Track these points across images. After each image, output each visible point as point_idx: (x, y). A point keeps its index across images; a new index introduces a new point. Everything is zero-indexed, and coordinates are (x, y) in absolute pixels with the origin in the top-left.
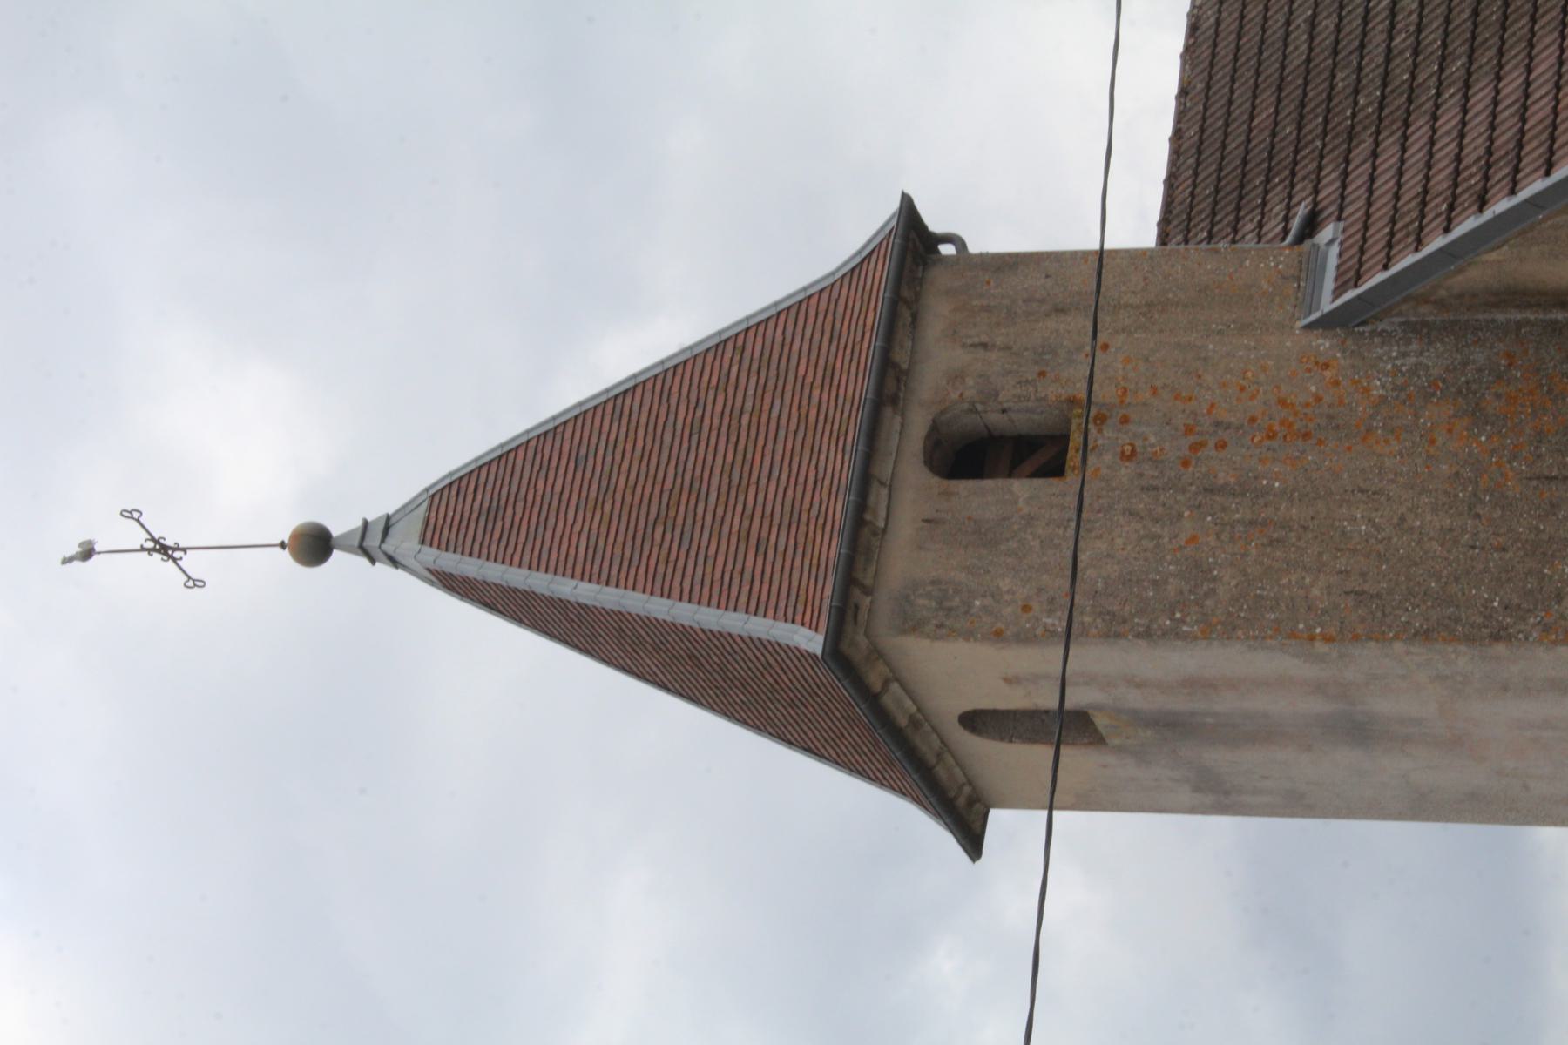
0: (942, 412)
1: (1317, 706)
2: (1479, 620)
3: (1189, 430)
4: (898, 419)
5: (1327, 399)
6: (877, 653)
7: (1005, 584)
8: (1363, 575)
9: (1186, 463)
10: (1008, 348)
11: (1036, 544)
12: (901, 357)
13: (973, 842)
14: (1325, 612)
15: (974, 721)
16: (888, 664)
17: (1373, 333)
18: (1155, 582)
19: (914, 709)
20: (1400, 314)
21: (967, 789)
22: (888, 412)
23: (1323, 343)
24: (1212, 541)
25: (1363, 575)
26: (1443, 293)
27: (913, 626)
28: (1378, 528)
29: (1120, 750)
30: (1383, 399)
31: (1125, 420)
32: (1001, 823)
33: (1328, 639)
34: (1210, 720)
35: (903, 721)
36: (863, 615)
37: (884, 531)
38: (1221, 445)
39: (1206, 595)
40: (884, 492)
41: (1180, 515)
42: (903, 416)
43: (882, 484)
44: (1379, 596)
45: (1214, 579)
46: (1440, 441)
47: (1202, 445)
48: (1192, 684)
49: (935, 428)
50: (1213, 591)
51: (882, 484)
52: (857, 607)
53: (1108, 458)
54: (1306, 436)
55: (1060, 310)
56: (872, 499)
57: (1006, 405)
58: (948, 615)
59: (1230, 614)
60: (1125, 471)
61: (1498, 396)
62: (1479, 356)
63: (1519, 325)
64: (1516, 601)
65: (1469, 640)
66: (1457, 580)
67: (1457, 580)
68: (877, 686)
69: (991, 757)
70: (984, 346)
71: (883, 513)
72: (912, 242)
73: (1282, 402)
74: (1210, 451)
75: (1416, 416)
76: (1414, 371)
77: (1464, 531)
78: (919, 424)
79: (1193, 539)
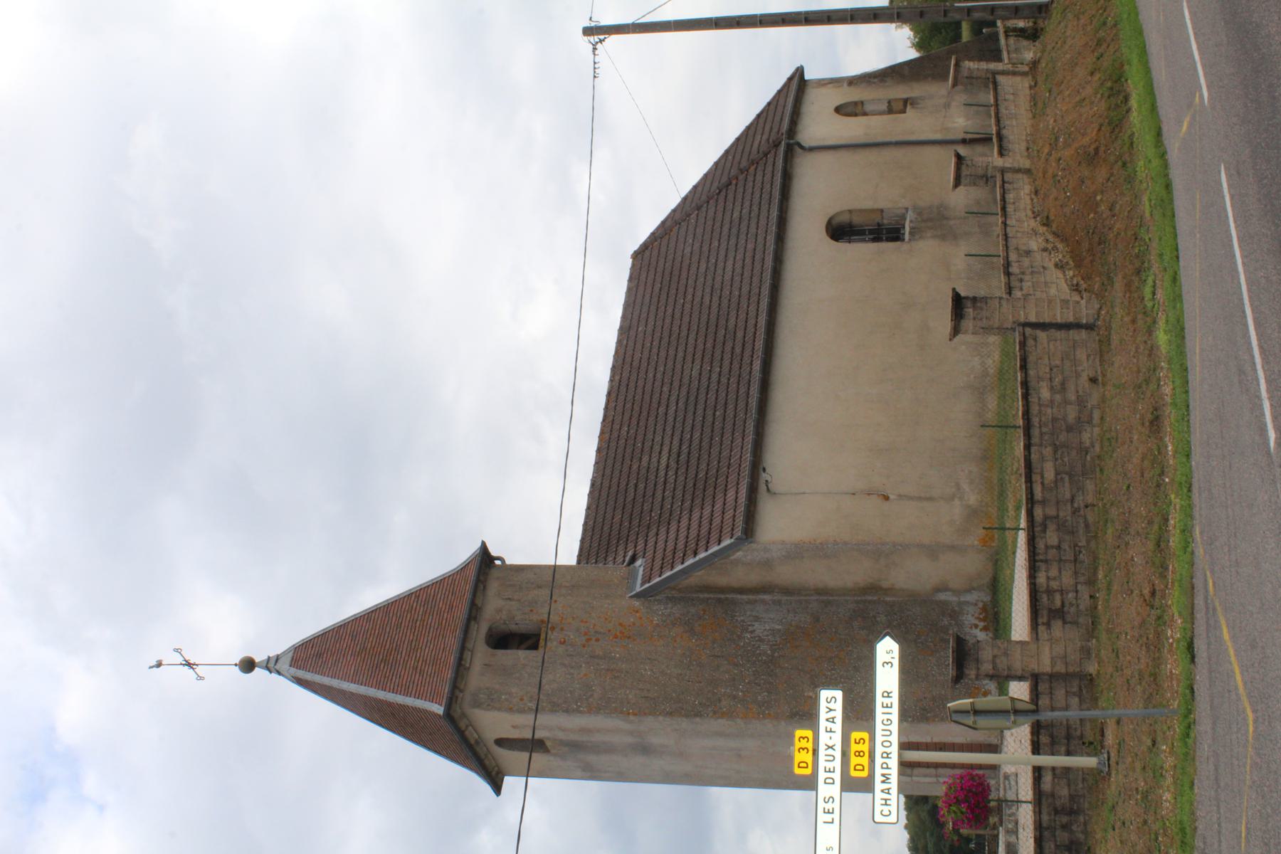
3: (586, 634)
6: (464, 715)
12: (478, 602)
15: (500, 742)
23: (637, 603)
27: (477, 704)
29: (555, 755)
31: (562, 629)
33: (635, 714)
35: (472, 742)
48: (583, 730)
58: (492, 701)
60: (561, 649)
62: (693, 610)
65: (687, 716)
72: (485, 559)
74: (593, 642)
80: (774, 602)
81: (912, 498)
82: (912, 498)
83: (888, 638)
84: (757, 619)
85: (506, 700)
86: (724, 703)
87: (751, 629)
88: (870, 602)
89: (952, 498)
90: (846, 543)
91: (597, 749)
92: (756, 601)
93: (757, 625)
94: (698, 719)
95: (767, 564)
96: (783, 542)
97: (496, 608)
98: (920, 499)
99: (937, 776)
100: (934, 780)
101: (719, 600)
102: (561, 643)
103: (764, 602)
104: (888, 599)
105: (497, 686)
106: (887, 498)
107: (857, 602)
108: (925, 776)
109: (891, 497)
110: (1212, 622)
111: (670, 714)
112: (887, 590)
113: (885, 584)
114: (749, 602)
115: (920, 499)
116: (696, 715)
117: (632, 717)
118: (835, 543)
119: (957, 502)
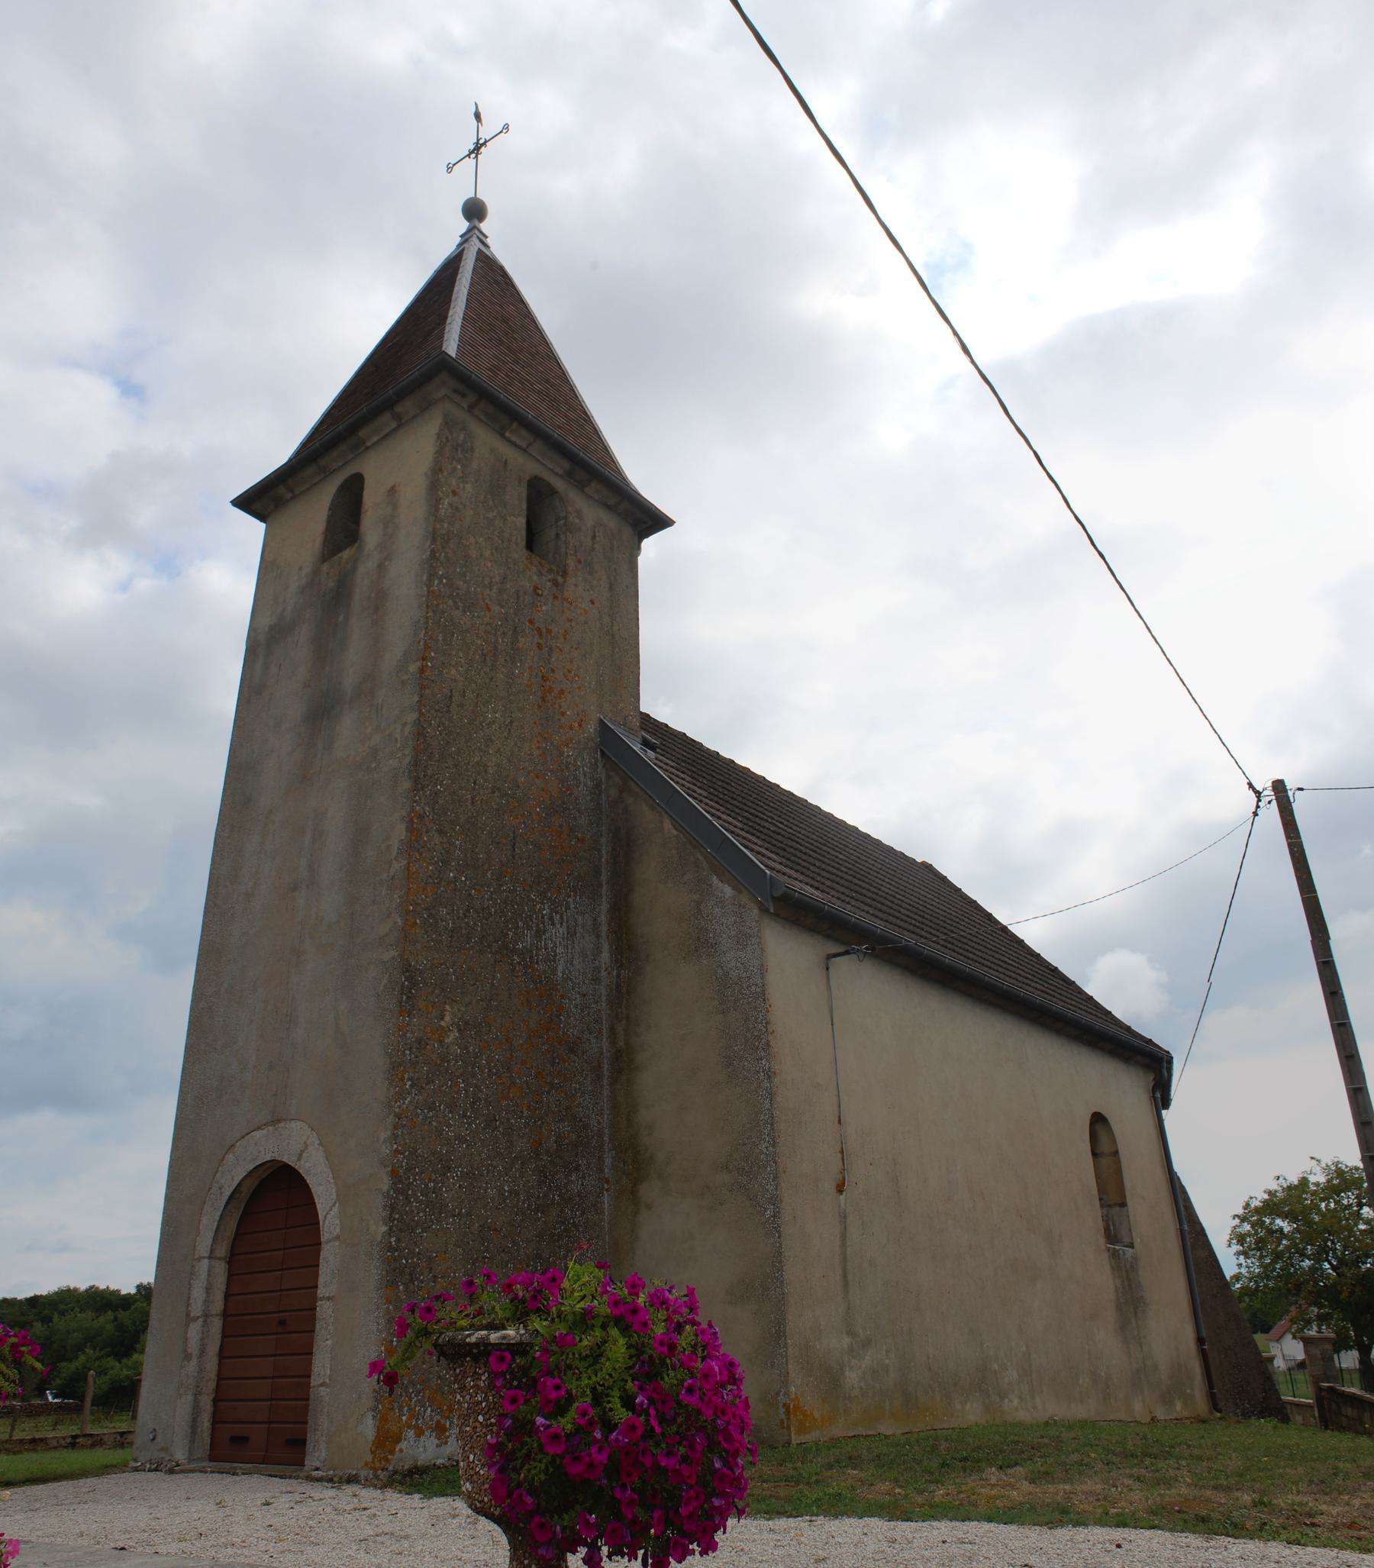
0: (561, 499)
1: (350, 679)
2: (429, 772)
3: (549, 632)
4: (561, 472)
5: (563, 720)
6: (425, 408)
7: (469, 487)
8: (461, 706)
9: (531, 622)
10: (593, 549)
11: (490, 515)
12: (594, 488)
13: (252, 502)
14: (441, 673)
15: (353, 489)
16: (415, 417)
17: (597, 760)
18: (464, 575)
19: (368, 444)
20: (608, 777)
21: (289, 495)
22: (567, 465)
23: (592, 728)
24: (487, 620)
25: (461, 706)
26: (630, 800)
27: (448, 424)
28: (490, 724)
29: (316, 572)
30: (562, 754)
31: (555, 597)
32: (253, 530)
33: (422, 670)
34: (341, 618)
35: (363, 433)
36: (457, 398)
37: (502, 435)
38: (540, 647)
39: (455, 603)
40: (524, 445)
41: (502, 607)
42: (561, 476)
43: (530, 444)
44: (448, 711)
45: (464, 612)
46: (538, 782)
47: (540, 635)
48: (379, 601)
49: (553, 492)
50: (457, 608)
51: (530, 444)
52: (464, 395)
53: (535, 578)
54: (543, 699)
55: (611, 587)
56: (524, 432)
57: (563, 537)
58: (452, 449)
59: (443, 612)
60: (527, 585)
61: (561, 826)
62: (583, 821)
63: (599, 851)
64: (441, 802)
65: (416, 763)
66: (455, 766)
67: (455, 766)
68: (398, 409)
69: (313, 514)
70: (594, 537)
71: (513, 439)
72: (653, 521)
73: (562, 692)
74: (537, 639)
75: (551, 771)
76: (576, 778)
77: (485, 780)
78: (559, 484)
79: (489, 609)
80: (597, 970)
81: (844, 1237)
82: (844, 1237)
83: (148, 1277)
84: (571, 933)
85: (455, 469)
86: (437, 839)
87: (557, 918)
88: (601, 1159)
89: (851, 1333)
90: (771, 1096)
91: (326, 648)
92: (598, 936)
93: (563, 930)
94: (407, 785)
95: (701, 944)
96: (763, 969)
97: (586, 512)
98: (844, 1259)
99: (206, 1315)
100: (197, 1309)
101: (597, 872)
102: (536, 588)
103: (598, 951)
104: (606, 1199)
105: (475, 465)
106: (840, 1189)
107: (600, 1135)
108: (208, 1290)
109: (842, 1197)
110: (55, 1443)
111: (420, 733)
112: (634, 1192)
113: (649, 1191)
114: (596, 924)
115: (844, 1259)
116: (416, 781)
117: (413, 668)
118: (770, 1075)
119: (846, 1341)
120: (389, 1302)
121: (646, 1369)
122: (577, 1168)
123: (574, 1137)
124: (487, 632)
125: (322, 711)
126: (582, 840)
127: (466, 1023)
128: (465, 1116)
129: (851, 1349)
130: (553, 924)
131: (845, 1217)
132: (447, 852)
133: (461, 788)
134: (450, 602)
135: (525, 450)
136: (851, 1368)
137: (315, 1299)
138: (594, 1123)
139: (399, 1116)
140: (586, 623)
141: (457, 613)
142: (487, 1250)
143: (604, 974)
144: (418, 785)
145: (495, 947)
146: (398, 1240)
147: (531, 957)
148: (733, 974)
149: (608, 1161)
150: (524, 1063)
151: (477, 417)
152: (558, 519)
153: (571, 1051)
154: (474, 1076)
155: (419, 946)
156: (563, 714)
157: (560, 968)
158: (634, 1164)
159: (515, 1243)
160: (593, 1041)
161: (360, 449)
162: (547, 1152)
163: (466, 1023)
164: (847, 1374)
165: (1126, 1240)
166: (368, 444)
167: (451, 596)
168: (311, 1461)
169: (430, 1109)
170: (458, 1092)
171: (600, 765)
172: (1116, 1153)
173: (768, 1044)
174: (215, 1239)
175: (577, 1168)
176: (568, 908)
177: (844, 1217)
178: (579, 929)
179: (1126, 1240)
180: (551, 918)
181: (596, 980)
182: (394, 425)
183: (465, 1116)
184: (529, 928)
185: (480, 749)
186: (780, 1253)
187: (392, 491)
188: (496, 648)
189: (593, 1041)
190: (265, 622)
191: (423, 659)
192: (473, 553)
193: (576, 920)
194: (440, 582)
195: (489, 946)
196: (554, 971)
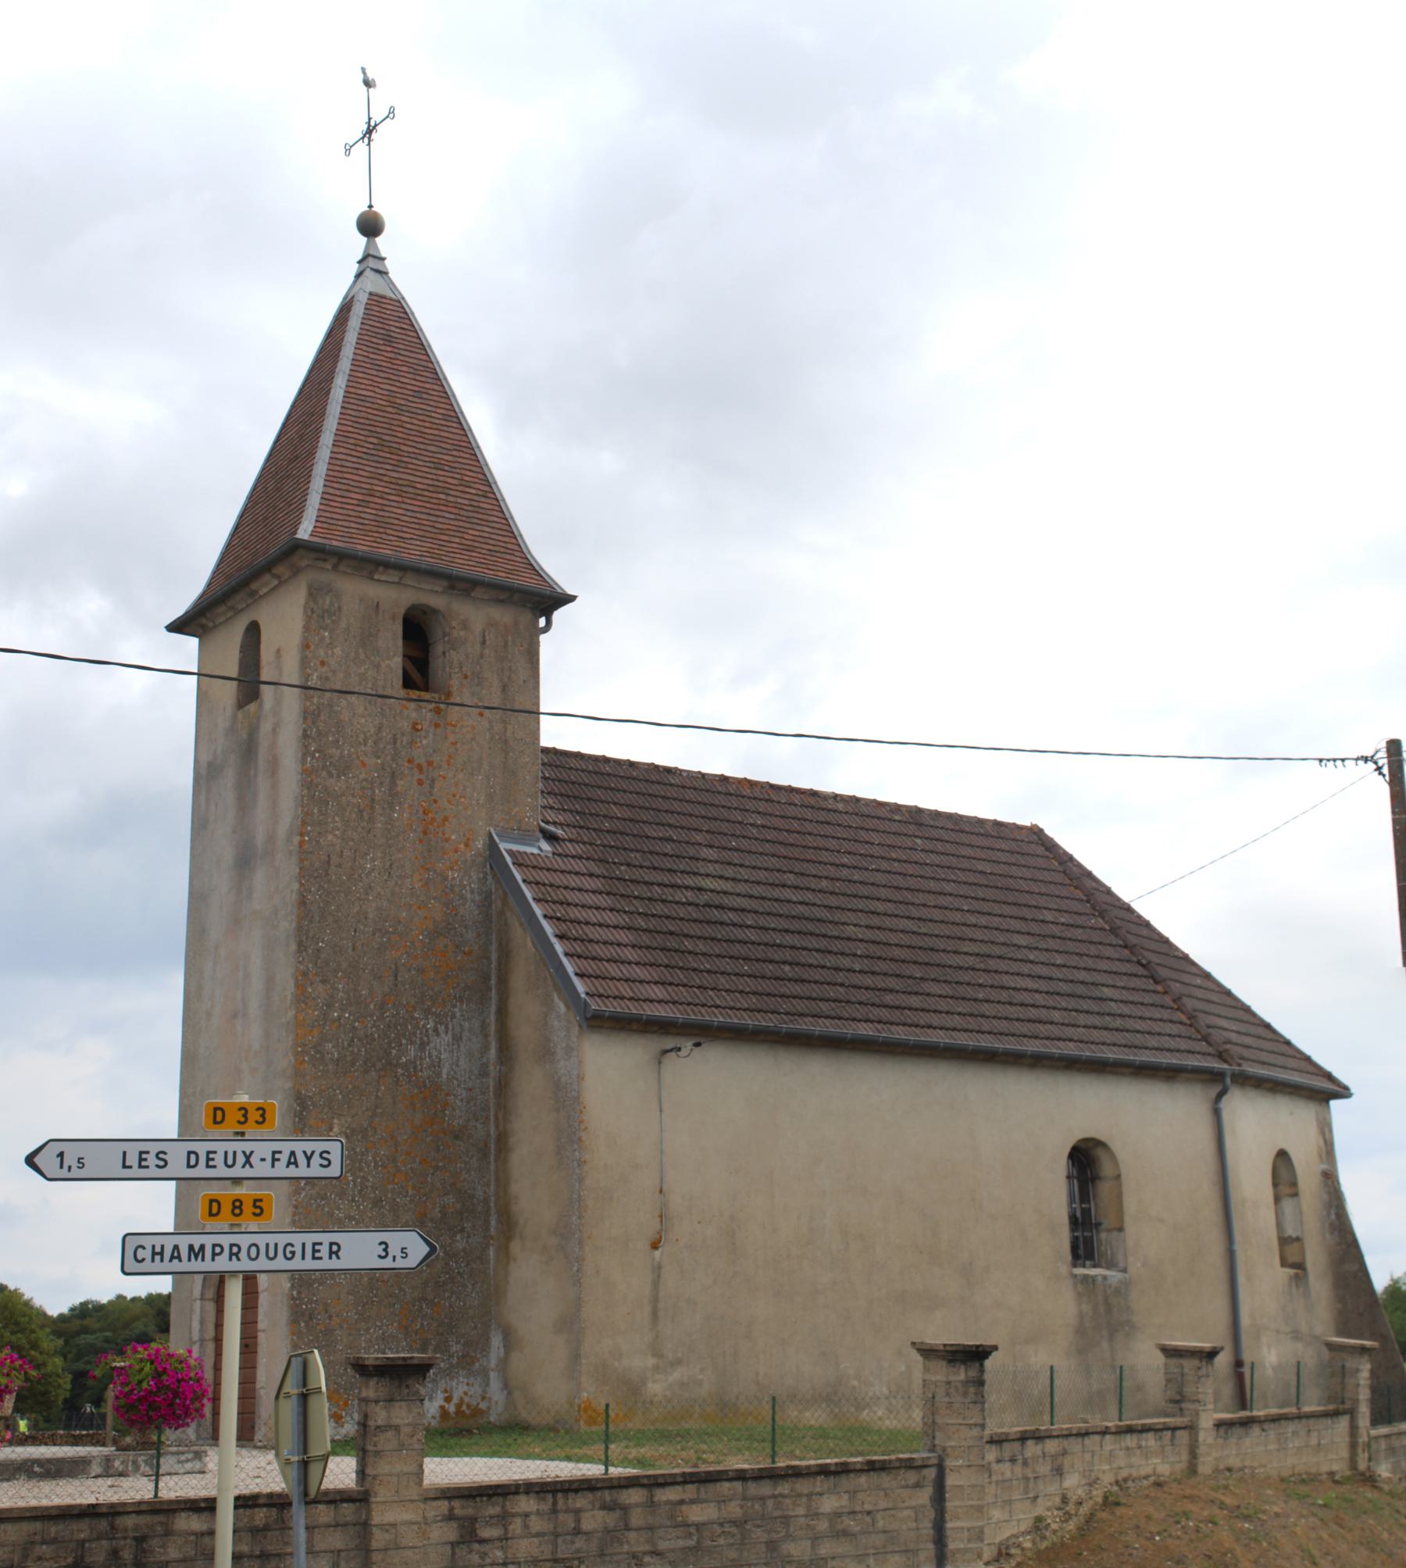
1: (260, 838)
3: (430, 763)
6: (296, 572)
7: (338, 651)
8: (339, 866)
10: (482, 656)
12: (478, 593)
19: (261, 593)
22: (445, 583)
27: (313, 593)
29: (235, 717)
30: (446, 879)
31: (437, 726)
32: (191, 644)
33: (301, 844)
36: (320, 564)
37: (372, 579)
38: (420, 782)
40: (396, 579)
44: (327, 874)
45: (339, 777)
48: (274, 765)
52: (325, 560)
53: (414, 715)
56: (391, 571)
58: (319, 616)
62: (470, 935)
63: (489, 959)
66: (336, 922)
69: (232, 638)
72: (549, 600)
73: (446, 819)
77: (365, 926)
79: (364, 765)
80: (485, 1065)
84: (457, 1039)
85: (322, 639)
87: (441, 1028)
88: (487, 1222)
92: (486, 1036)
93: (448, 1038)
95: (546, 1053)
96: (581, 1078)
97: (470, 622)
99: (202, 1341)
100: (196, 1336)
101: (486, 978)
103: (486, 1048)
104: (491, 1252)
107: (486, 1201)
108: (202, 1322)
109: (657, 1253)
111: (302, 902)
112: (507, 1248)
113: (515, 1247)
114: (484, 1026)
117: (296, 839)
118: (581, 1163)
119: (650, 1362)
120: (293, 1334)
121: (157, 1376)
122: (462, 1230)
123: (458, 1206)
124: (363, 788)
125: (244, 862)
126: (470, 953)
127: (353, 1131)
128: (353, 1200)
129: (656, 1369)
130: (438, 1035)
131: (660, 1267)
132: (332, 996)
133: (342, 939)
134: (324, 773)
135: (398, 583)
136: (655, 1381)
137: (256, 1331)
138: (479, 1193)
139: (296, 1207)
140: (473, 739)
141: (332, 781)
142: (376, 1296)
143: (491, 1068)
144: (301, 947)
145: (379, 1065)
146: (299, 1293)
147: (415, 1068)
148: (563, 1080)
149: (493, 1223)
150: (408, 1154)
151: (345, 573)
152: (444, 635)
153: (456, 1137)
154: (361, 1169)
155: (308, 1078)
156: (447, 840)
157: (445, 1072)
158: (508, 1226)
159: (401, 1289)
160: (479, 1126)
161: (255, 598)
162: (432, 1220)
163: (353, 1131)
164: (650, 1385)
165: (1121, 1265)
166: (261, 593)
167: (324, 767)
168: (258, 1436)
169: (322, 1199)
170: (348, 1184)
171: (490, 878)
172: (1118, 1177)
173: (580, 1139)
174: (204, 1286)
175: (462, 1230)
176: (453, 1016)
177: (658, 1269)
178: (466, 1034)
179: (1121, 1265)
180: (436, 1030)
181: (484, 1073)
182: (276, 582)
183: (353, 1200)
184: (412, 1043)
185: (359, 899)
186: (579, 1298)
187: (278, 651)
188: (373, 800)
189: (479, 1126)
190: (205, 758)
191: (302, 835)
192: (345, 716)
193: (462, 1027)
194: (313, 757)
195: (374, 1065)
196: (439, 1075)
